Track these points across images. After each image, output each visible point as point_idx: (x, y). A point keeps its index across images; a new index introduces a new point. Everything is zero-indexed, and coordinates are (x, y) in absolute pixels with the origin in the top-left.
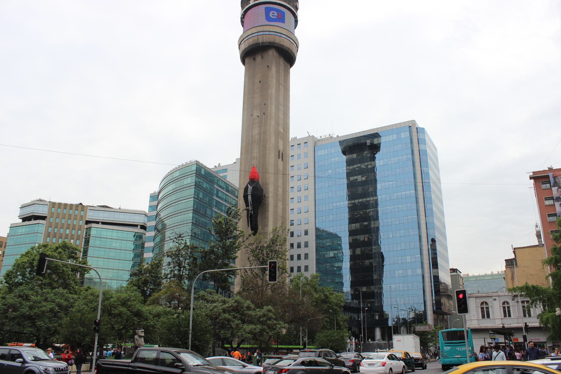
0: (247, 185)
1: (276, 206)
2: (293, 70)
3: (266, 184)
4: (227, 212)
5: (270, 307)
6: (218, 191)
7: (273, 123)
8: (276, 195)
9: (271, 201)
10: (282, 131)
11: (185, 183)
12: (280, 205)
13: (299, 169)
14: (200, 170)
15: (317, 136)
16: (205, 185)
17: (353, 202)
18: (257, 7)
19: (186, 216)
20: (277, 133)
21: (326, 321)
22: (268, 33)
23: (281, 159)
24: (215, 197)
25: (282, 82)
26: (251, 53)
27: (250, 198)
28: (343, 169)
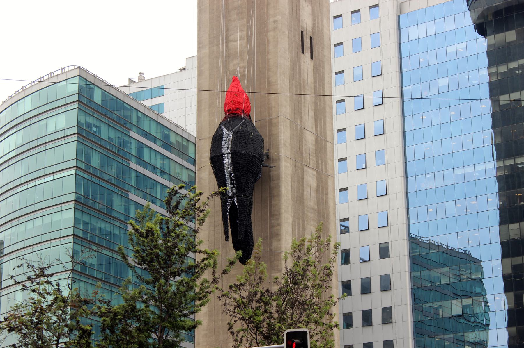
1: (299, 182)
3: (271, 124)
4: (168, 203)
6: (141, 146)
8: (299, 151)
9: (285, 169)
12: (311, 179)
13: (359, 79)
14: (91, 92)
16: (106, 133)
19: (57, 217)
23: (308, 54)
24: (133, 165)
27: (227, 162)
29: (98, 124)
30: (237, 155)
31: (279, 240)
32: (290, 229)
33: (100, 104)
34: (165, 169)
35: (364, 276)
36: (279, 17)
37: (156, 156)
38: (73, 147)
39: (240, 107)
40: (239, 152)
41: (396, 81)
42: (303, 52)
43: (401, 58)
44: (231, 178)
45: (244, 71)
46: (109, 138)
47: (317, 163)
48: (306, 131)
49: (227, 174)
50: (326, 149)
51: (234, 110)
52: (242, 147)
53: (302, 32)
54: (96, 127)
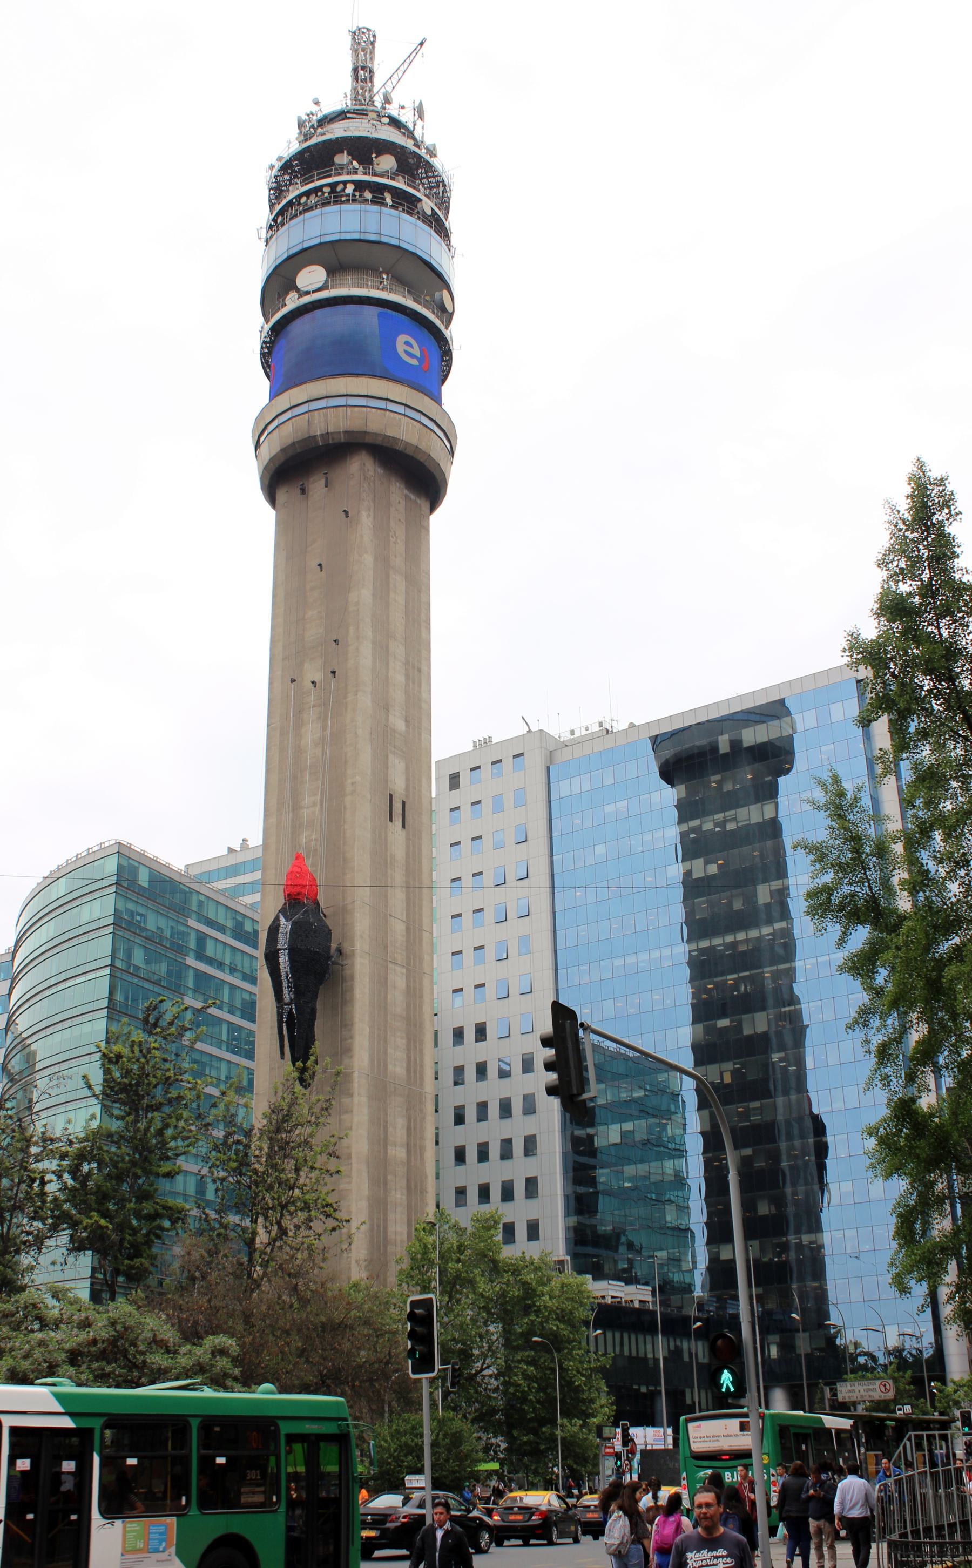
0: (277, 919)
1: (381, 982)
2: (437, 520)
3: (344, 911)
4: (146, 1020)
5: (222, 1340)
6: (202, 939)
7: (365, 701)
8: (382, 943)
9: (361, 970)
10: (400, 725)
11: (85, 919)
12: (398, 979)
13: (499, 846)
14: (134, 871)
15: (559, 729)
17: (704, 944)
18: (307, 317)
19: (87, 1028)
20: (383, 738)
21: (526, 1377)
22: (342, 401)
23: (398, 823)
24: (191, 961)
25: (398, 561)
26: (293, 470)
27: (284, 960)
28: (670, 833)
29: (141, 910)
31: (351, 1057)
32: (366, 1043)
35: (503, 1096)
36: (358, 778)
37: (224, 949)
39: (303, 891)
41: (544, 850)
42: (391, 820)
43: (550, 820)
44: (289, 982)
46: (158, 928)
47: (408, 958)
48: (393, 919)
49: (283, 974)
50: (421, 940)
53: (391, 795)
54: (141, 915)
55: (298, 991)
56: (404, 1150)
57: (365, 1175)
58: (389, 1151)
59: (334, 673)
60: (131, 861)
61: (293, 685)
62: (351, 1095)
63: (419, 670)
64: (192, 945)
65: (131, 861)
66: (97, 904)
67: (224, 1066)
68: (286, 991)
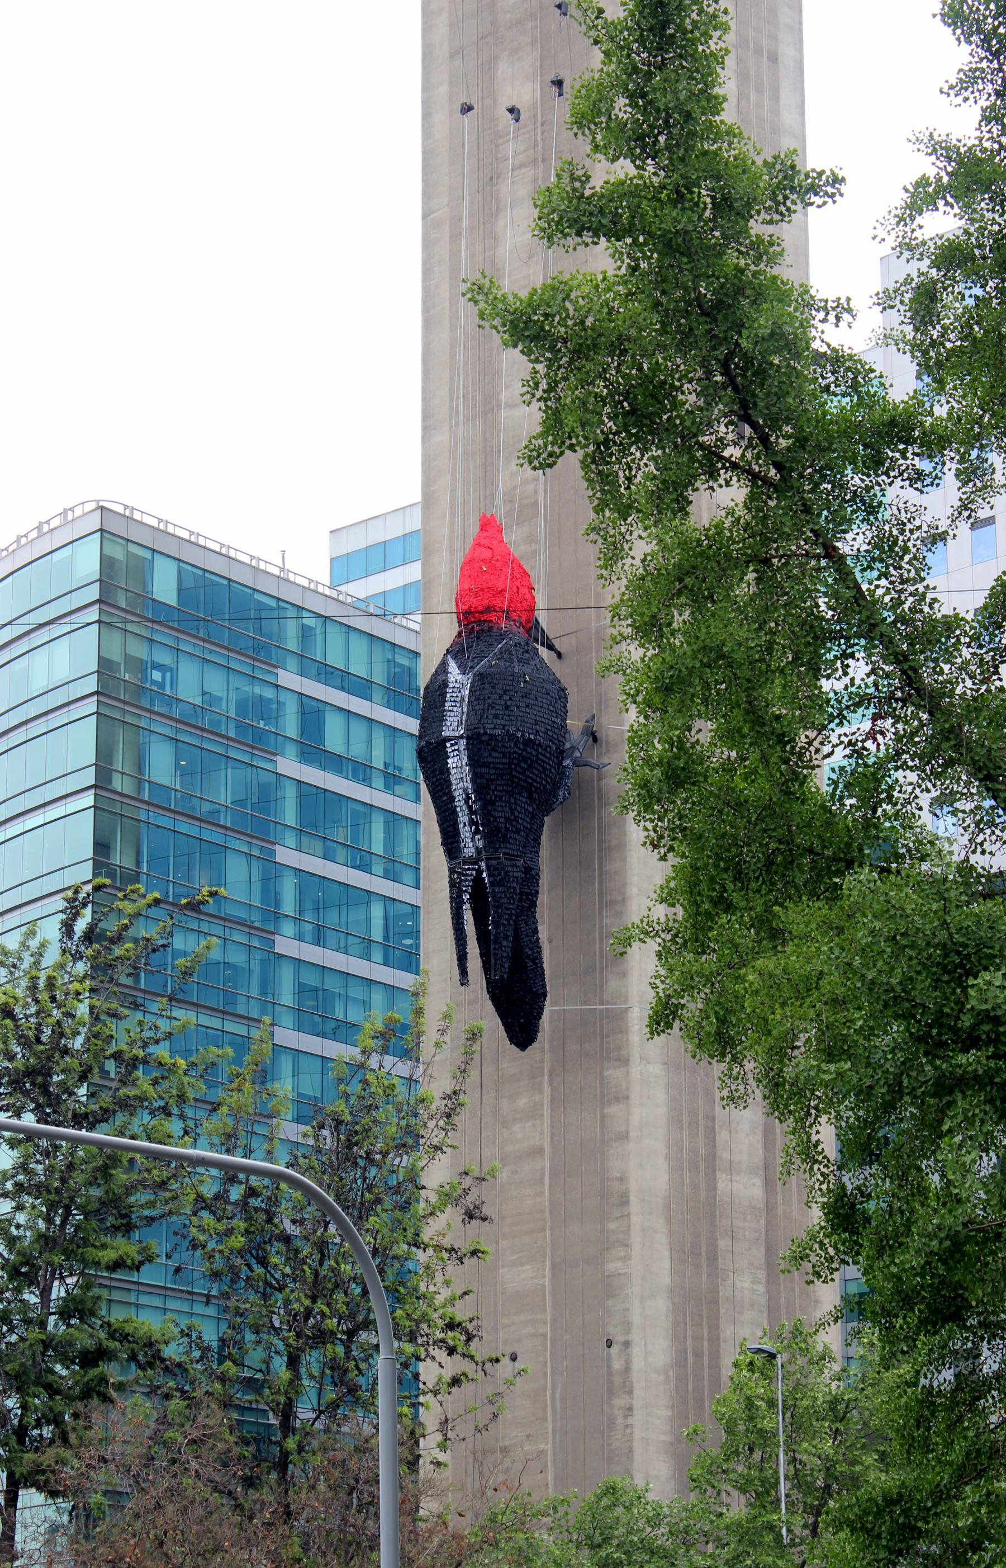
6: (312, 714)
11: (39, 682)
14: (142, 571)
16: (191, 682)
24: (289, 765)
27: (458, 764)
30: (482, 742)
31: (624, 974)
33: (174, 604)
34: (400, 770)
38: (86, 734)
39: (497, 602)
40: (485, 733)
44: (470, 808)
45: (536, 492)
49: (459, 795)
51: (481, 612)
52: (496, 716)
55: (493, 834)
56: (758, 1181)
57: (662, 1242)
58: (720, 1185)
59: (559, 83)
60: (132, 548)
61: (466, 119)
62: (626, 1062)
63: (774, 59)
64: (291, 727)
65: (132, 548)
66: (62, 647)
67: (378, 997)
68: (465, 832)
